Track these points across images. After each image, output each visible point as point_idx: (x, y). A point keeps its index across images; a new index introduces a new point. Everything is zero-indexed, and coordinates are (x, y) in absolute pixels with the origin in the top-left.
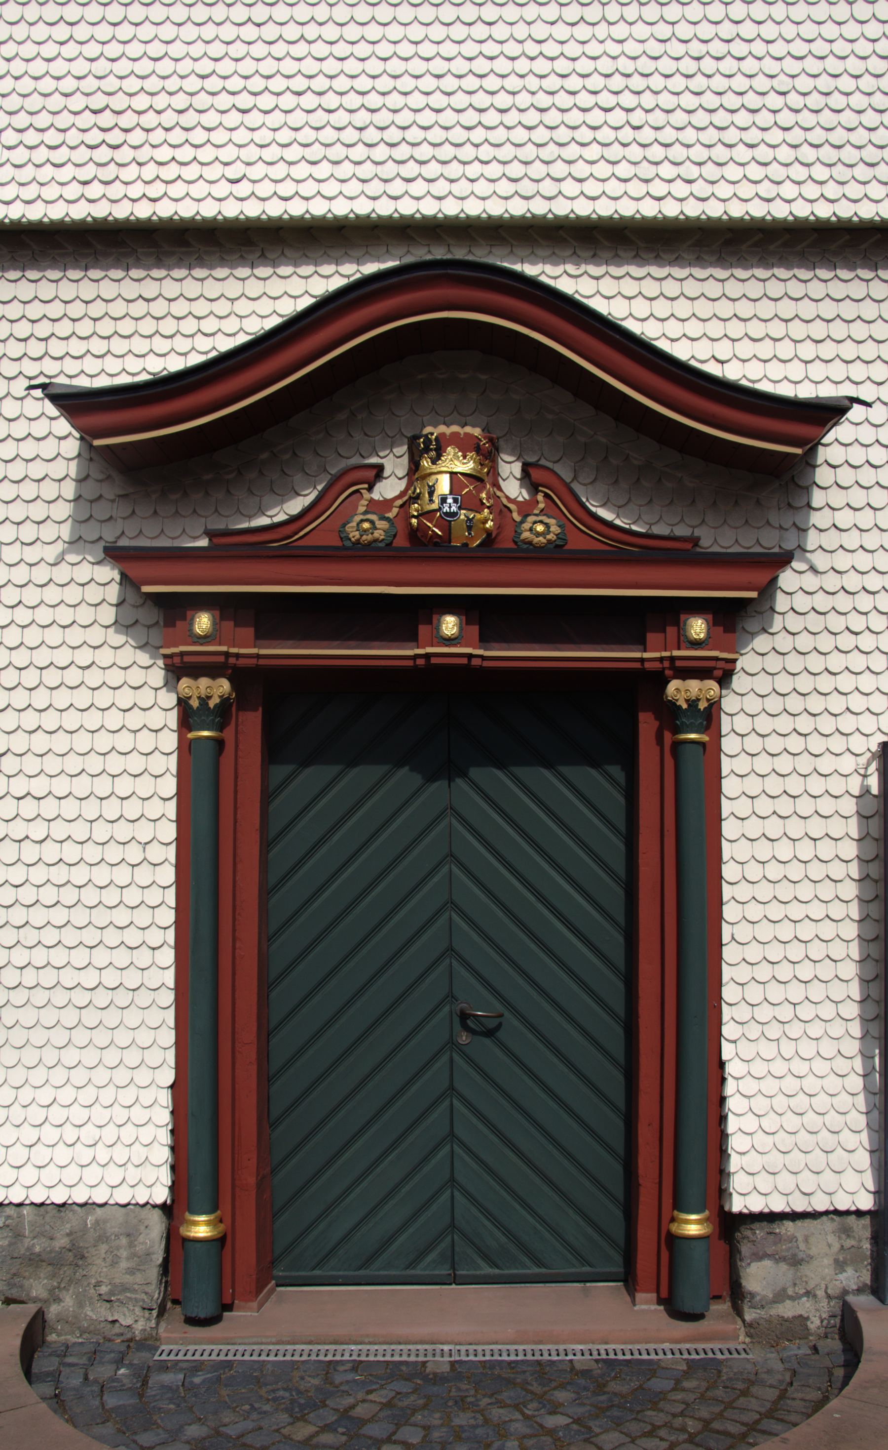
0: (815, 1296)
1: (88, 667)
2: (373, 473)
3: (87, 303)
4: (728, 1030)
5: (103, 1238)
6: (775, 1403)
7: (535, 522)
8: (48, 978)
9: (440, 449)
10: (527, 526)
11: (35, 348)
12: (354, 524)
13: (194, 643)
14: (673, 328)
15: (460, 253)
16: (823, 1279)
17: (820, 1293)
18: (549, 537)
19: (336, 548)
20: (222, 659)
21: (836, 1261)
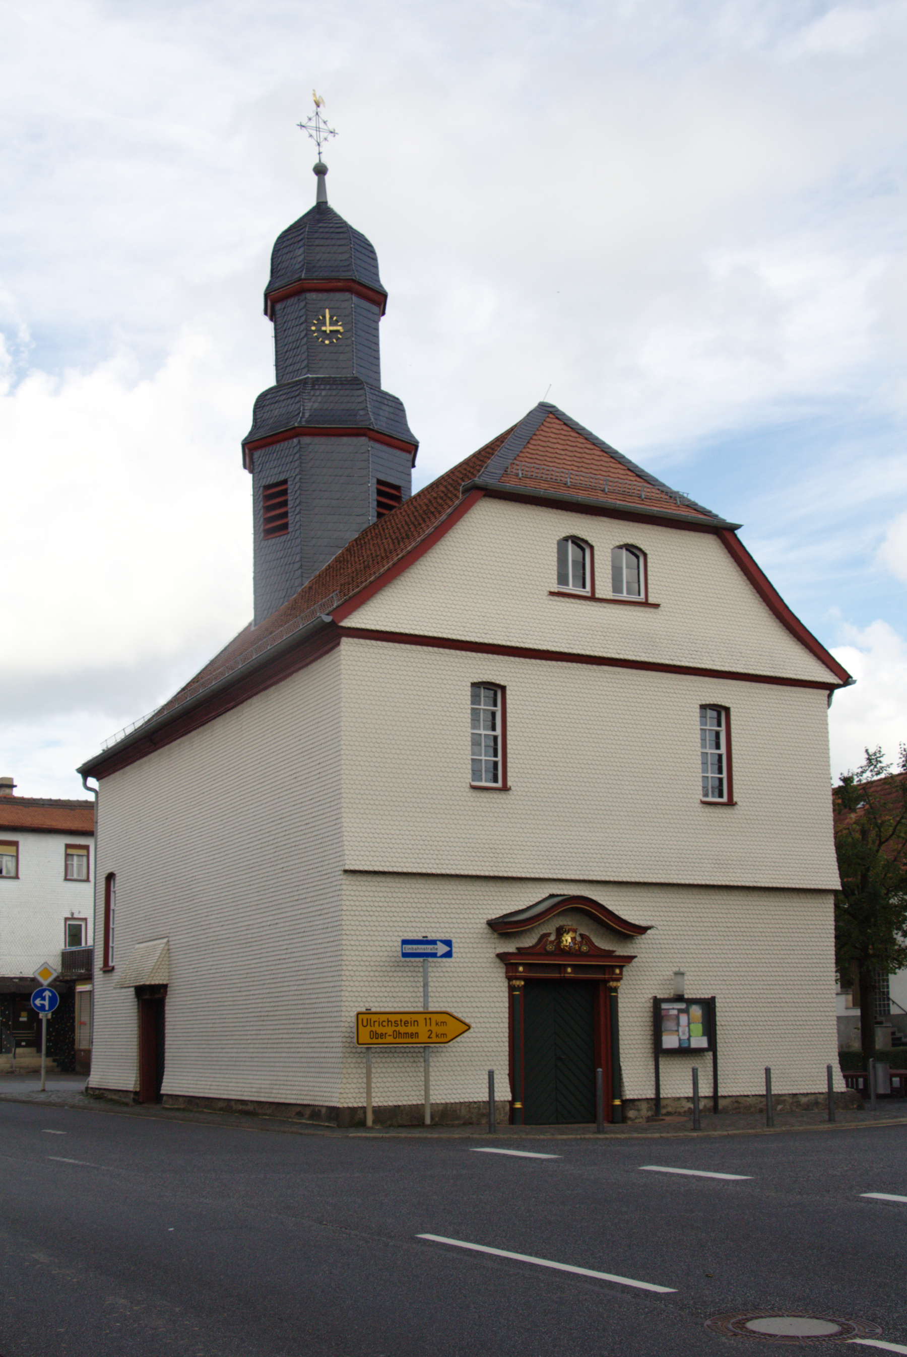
4: (621, 1059)
14: (625, 913)
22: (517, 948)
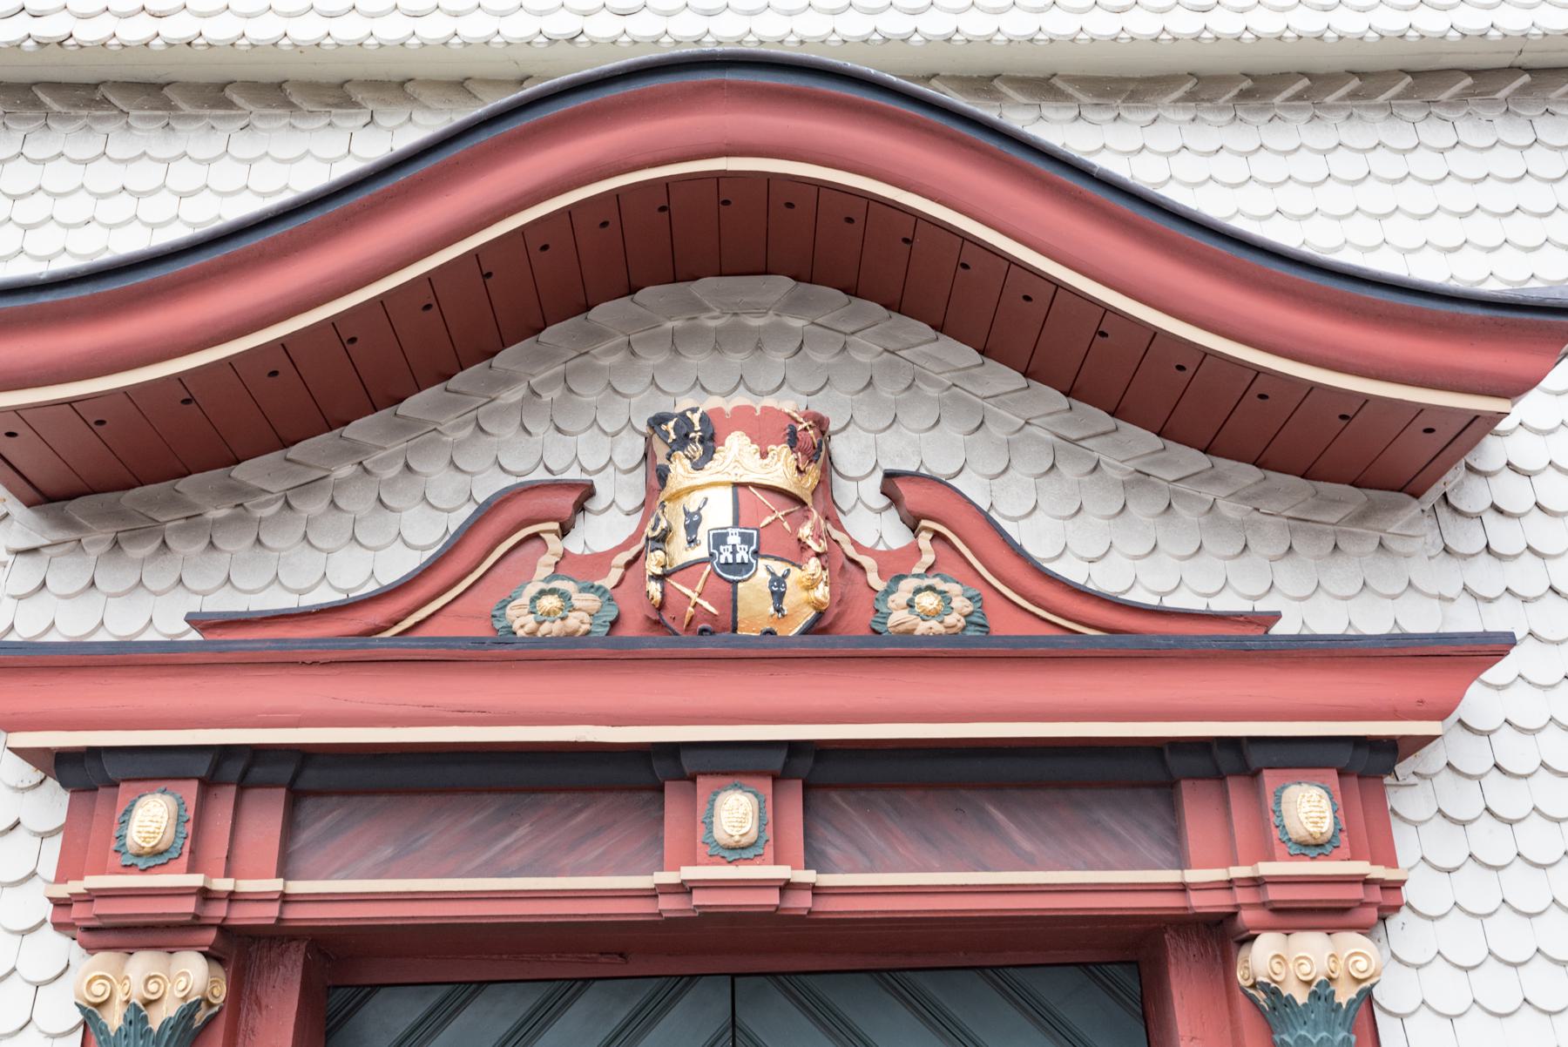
7: (918, 591)
9: (712, 438)
12: (525, 600)
13: (128, 868)
18: (951, 620)
19: (479, 642)
20: (188, 906)
22: (194, 620)
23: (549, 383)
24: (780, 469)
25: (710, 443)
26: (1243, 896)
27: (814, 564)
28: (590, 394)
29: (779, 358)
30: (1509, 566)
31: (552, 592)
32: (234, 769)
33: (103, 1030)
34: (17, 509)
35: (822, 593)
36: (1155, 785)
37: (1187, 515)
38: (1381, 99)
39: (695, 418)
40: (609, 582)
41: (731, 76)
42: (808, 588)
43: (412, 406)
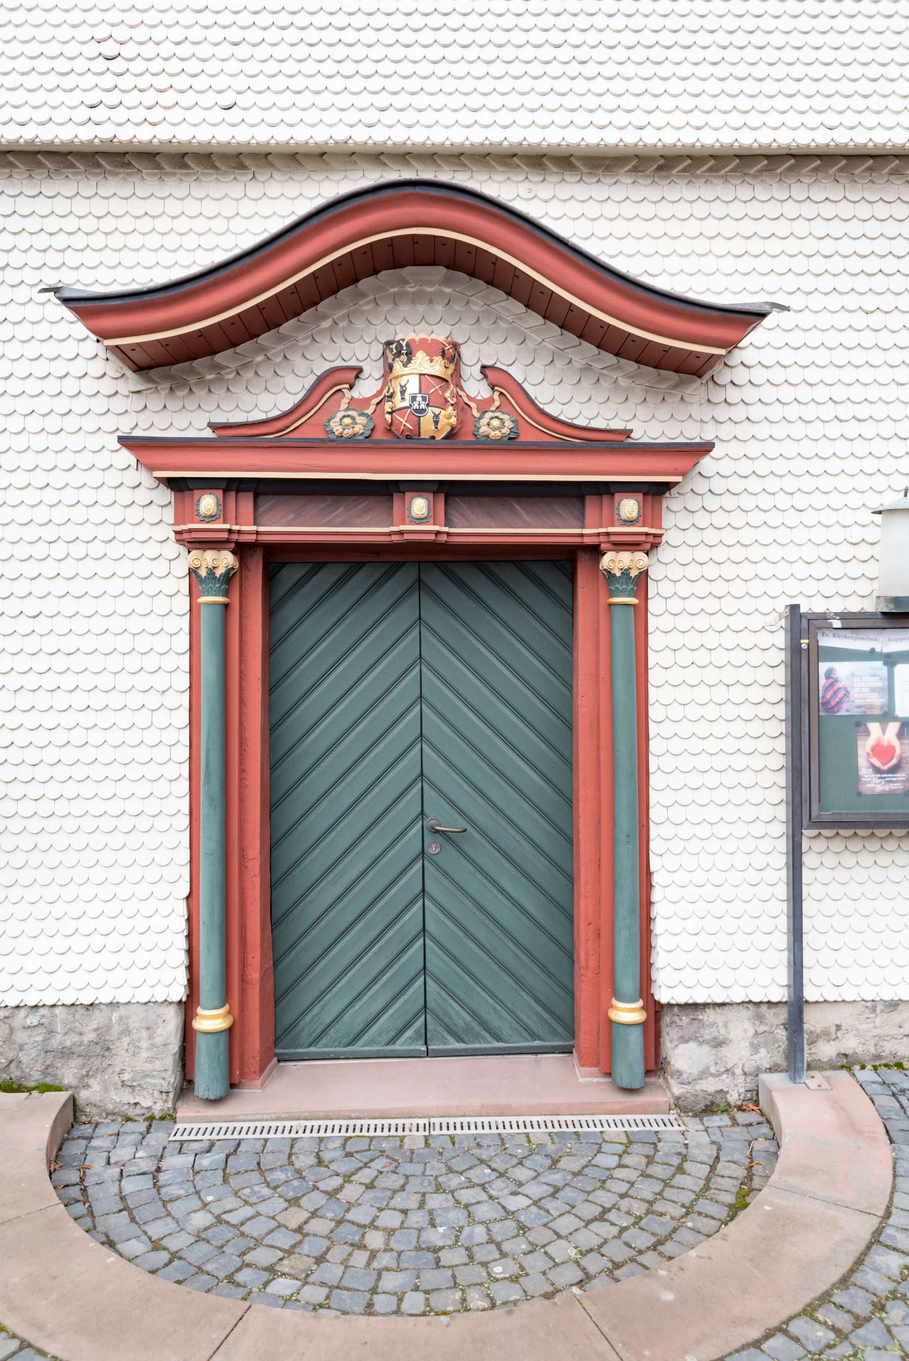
0: (734, 1074)
1: (111, 541)
2: (354, 374)
3: (99, 218)
5: (126, 1032)
6: (708, 1179)
8: (78, 807)
10: (484, 421)
11: (53, 259)
12: (337, 419)
13: (202, 521)
15: (427, 174)
16: (741, 1059)
17: (738, 1071)
18: (503, 431)
19: (323, 440)
20: (225, 535)
21: (752, 1044)
22: (214, 427)
23: (342, 318)
24: (437, 367)
25: (410, 355)
26: (602, 539)
27: (450, 408)
28: (359, 324)
29: (439, 308)
30: (733, 408)
31: (348, 416)
32: (235, 485)
33: (199, 576)
34: (129, 373)
35: (453, 420)
36: (576, 497)
37: (604, 384)
38: (722, 172)
39: (404, 344)
40: (370, 411)
41: (418, 190)
42: (448, 418)
43: (285, 328)
